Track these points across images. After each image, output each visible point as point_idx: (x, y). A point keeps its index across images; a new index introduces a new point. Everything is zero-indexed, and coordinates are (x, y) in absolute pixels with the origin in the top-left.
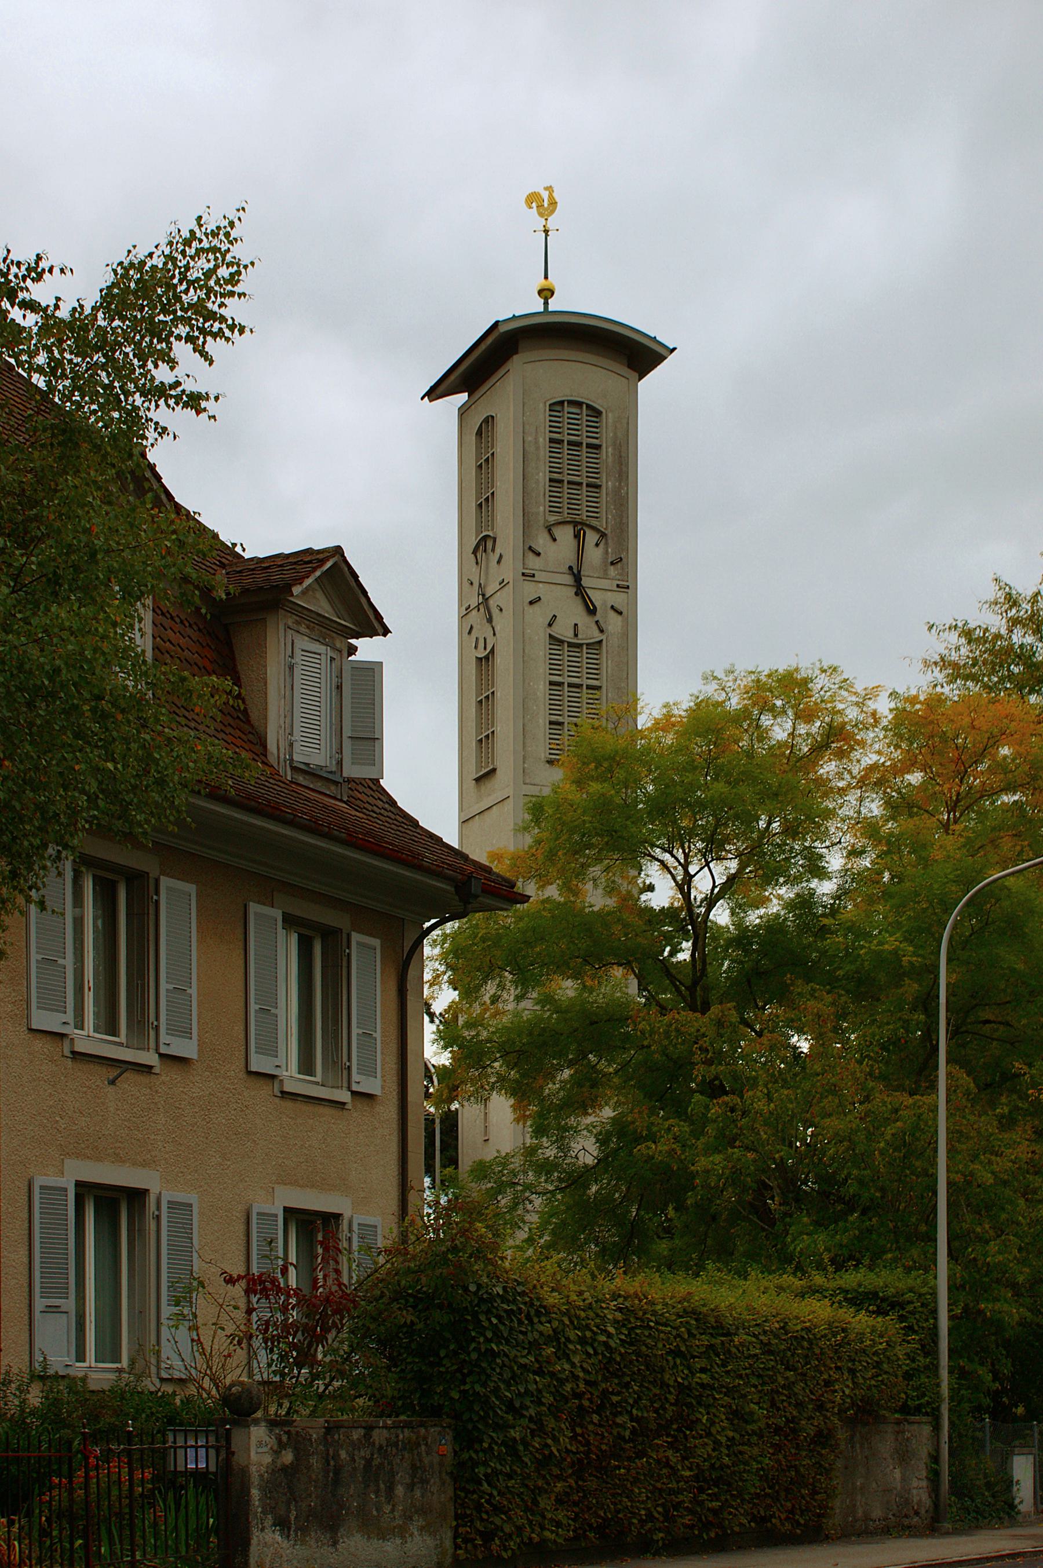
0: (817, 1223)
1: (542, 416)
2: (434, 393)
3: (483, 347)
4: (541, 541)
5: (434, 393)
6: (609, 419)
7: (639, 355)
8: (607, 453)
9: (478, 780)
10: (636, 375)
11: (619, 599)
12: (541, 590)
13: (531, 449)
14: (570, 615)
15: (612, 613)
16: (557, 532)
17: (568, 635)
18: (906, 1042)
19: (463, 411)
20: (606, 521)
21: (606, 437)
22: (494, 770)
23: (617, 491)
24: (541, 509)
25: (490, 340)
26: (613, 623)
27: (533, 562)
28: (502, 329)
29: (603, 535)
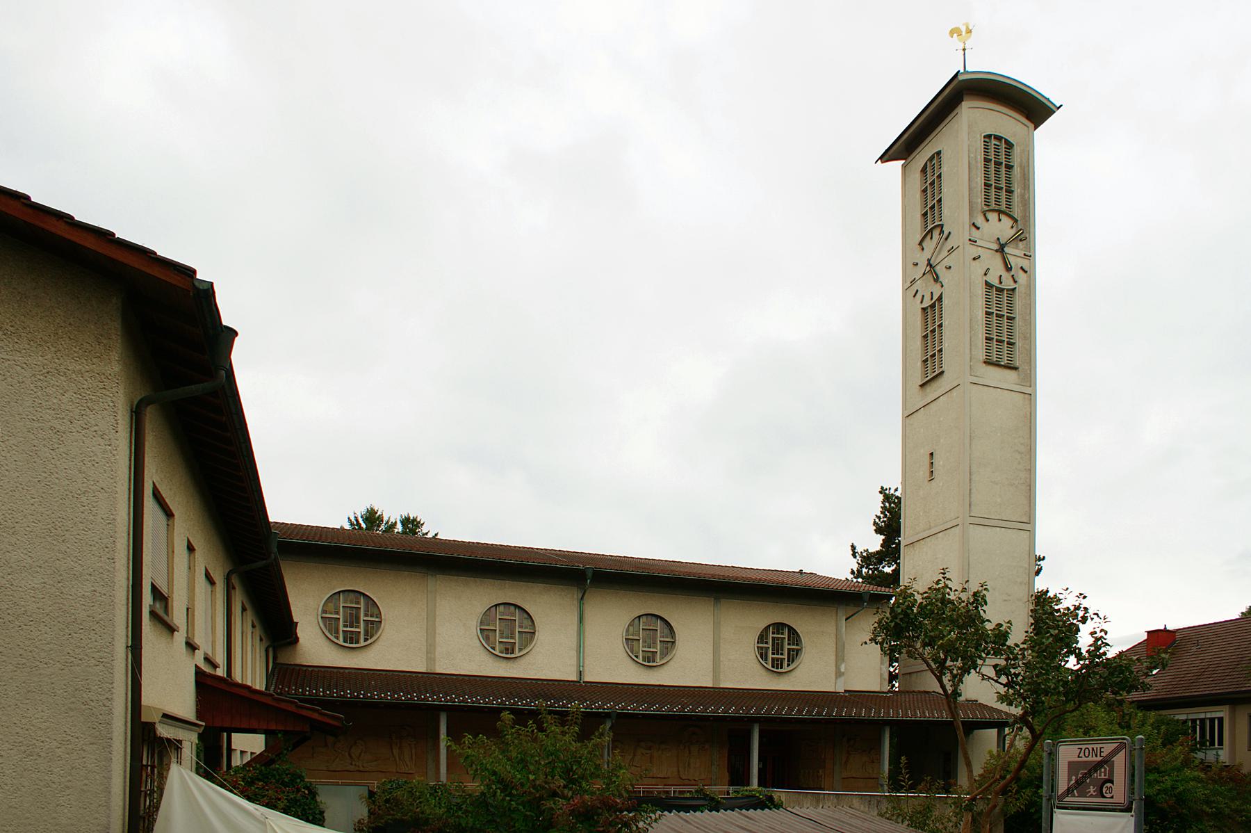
0: (1128, 668)
1: (980, 145)
2: (886, 157)
3: (940, 99)
4: (980, 220)
5: (886, 157)
6: (1017, 150)
7: (1034, 109)
8: (1017, 171)
9: (921, 386)
10: (1031, 126)
11: (1024, 263)
12: (980, 251)
13: (973, 162)
14: (997, 269)
15: (1021, 272)
16: (990, 215)
17: (995, 282)
18: (252, 783)
19: (904, 167)
20: (1017, 213)
21: (1016, 161)
22: (942, 372)
23: (1023, 196)
24: (980, 200)
25: (940, 99)
26: (1021, 277)
27: (975, 233)
28: (961, 78)
29: (1016, 221)
